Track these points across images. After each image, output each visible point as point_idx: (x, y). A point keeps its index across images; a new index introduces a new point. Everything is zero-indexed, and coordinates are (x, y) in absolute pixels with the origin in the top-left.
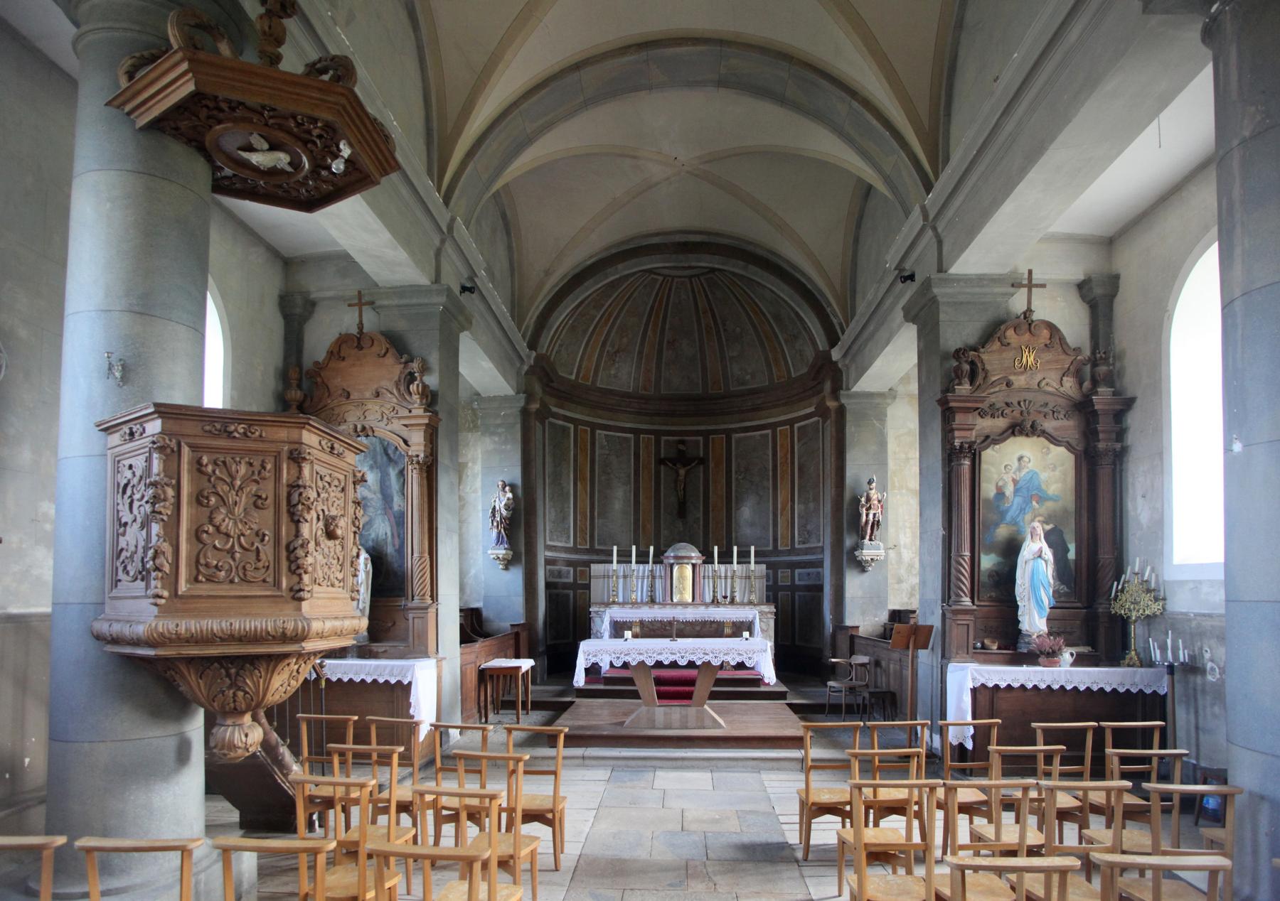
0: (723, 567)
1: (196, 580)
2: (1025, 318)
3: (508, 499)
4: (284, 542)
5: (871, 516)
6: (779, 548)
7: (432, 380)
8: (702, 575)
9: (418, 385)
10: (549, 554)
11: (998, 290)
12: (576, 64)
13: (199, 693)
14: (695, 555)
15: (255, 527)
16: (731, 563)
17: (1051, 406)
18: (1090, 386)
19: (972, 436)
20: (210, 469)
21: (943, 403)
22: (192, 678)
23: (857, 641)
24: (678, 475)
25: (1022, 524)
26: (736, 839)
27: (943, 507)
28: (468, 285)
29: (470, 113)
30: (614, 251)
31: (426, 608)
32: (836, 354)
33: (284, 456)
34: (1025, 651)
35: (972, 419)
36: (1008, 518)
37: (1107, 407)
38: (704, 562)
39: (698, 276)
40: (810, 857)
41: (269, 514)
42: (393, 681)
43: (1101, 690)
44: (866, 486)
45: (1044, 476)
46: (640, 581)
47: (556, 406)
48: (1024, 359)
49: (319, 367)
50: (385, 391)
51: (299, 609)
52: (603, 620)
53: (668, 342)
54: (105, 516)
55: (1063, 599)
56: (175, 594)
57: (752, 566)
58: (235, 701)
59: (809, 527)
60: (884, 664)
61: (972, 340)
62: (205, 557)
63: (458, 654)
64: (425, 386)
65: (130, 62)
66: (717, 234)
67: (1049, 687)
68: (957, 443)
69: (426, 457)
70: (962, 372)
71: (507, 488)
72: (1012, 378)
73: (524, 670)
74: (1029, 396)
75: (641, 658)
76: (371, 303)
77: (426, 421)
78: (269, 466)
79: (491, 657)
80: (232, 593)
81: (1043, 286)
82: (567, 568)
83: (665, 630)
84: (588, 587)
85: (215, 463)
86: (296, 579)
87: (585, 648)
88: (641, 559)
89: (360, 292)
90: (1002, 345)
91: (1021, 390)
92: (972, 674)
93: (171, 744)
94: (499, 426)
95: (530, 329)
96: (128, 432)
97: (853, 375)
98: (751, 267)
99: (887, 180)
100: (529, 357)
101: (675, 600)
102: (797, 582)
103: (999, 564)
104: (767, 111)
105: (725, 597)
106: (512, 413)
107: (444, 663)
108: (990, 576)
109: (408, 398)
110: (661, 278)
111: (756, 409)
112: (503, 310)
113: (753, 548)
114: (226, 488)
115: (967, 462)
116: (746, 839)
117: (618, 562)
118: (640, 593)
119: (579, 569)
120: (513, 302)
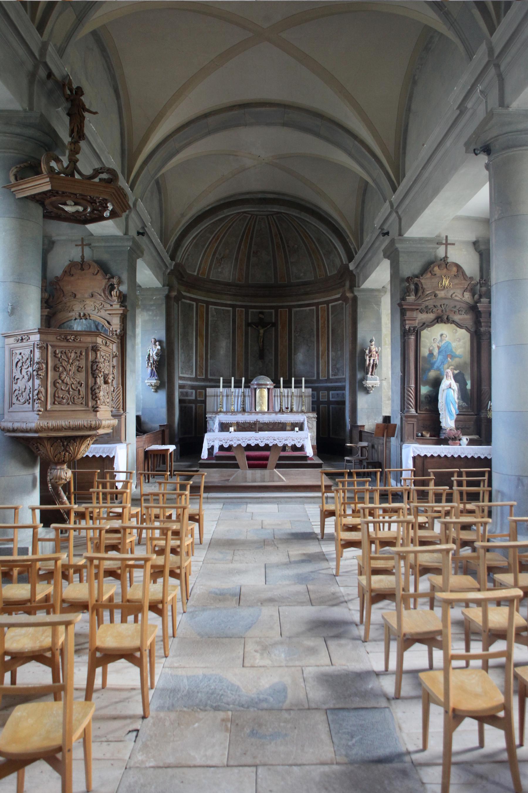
0: (286, 390)
1: (54, 403)
2: (444, 261)
3: (158, 350)
4: (90, 387)
5: (372, 361)
6: (320, 378)
7: (124, 288)
8: (273, 395)
9: (116, 292)
10: (181, 382)
11: (431, 246)
12: (205, 114)
13: (50, 453)
14: (269, 383)
15: (78, 380)
16: (291, 387)
17: (458, 307)
18: (478, 297)
19: (416, 323)
20: (59, 355)
21: (400, 305)
22: (48, 447)
23: (363, 434)
24: (259, 333)
25: (442, 370)
26: (289, 531)
27: (401, 361)
28: (141, 231)
29: (146, 142)
30: (222, 202)
31: (121, 416)
32: (352, 266)
33: (90, 349)
34: (443, 437)
35: (415, 314)
36: (435, 367)
37: (485, 309)
38: (275, 387)
39: (272, 215)
40: (324, 537)
41: (83, 374)
42: (104, 456)
43: (479, 457)
44: (369, 344)
45: (454, 345)
46: (236, 398)
47: (185, 291)
48: (444, 283)
49: (58, 280)
50: (97, 294)
51: (96, 416)
52: (215, 421)
53: (254, 252)
54: (4, 375)
55: (464, 410)
56: (46, 409)
57: (303, 389)
58: (64, 457)
59: (338, 366)
60: (376, 446)
61: (417, 272)
62: (58, 393)
63: (135, 442)
64: (120, 292)
65: (15, 170)
66: (284, 194)
67: (452, 456)
68: (407, 327)
69: (121, 331)
70: (410, 289)
71: (157, 343)
72: (437, 292)
73: (171, 451)
74: (446, 302)
75: (239, 442)
76: (89, 245)
77: (121, 312)
78: (84, 354)
79: (150, 444)
80: (69, 409)
81: (453, 244)
82: (191, 391)
83: (252, 428)
84: (204, 402)
85: (61, 353)
86: (95, 402)
87: (207, 436)
88: (237, 385)
89: (82, 239)
90: (432, 275)
91: (442, 298)
92: (413, 449)
93: (30, 478)
94: (152, 305)
95: (171, 248)
96: (20, 338)
97: (361, 278)
98: (303, 213)
99: (374, 181)
100: (171, 264)
101: (257, 410)
102: (331, 399)
103: (430, 391)
104: (309, 138)
105: (287, 408)
106: (160, 297)
107: (129, 446)
108: (426, 397)
109: (110, 298)
110: (250, 216)
111: (306, 294)
112: (157, 240)
113: (303, 379)
114: (66, 363)
115: (413, 338)
116: (294, 531)
117: (224, 387)
118: (236, 405)
119: (198, 391)
120: (161, 231)
